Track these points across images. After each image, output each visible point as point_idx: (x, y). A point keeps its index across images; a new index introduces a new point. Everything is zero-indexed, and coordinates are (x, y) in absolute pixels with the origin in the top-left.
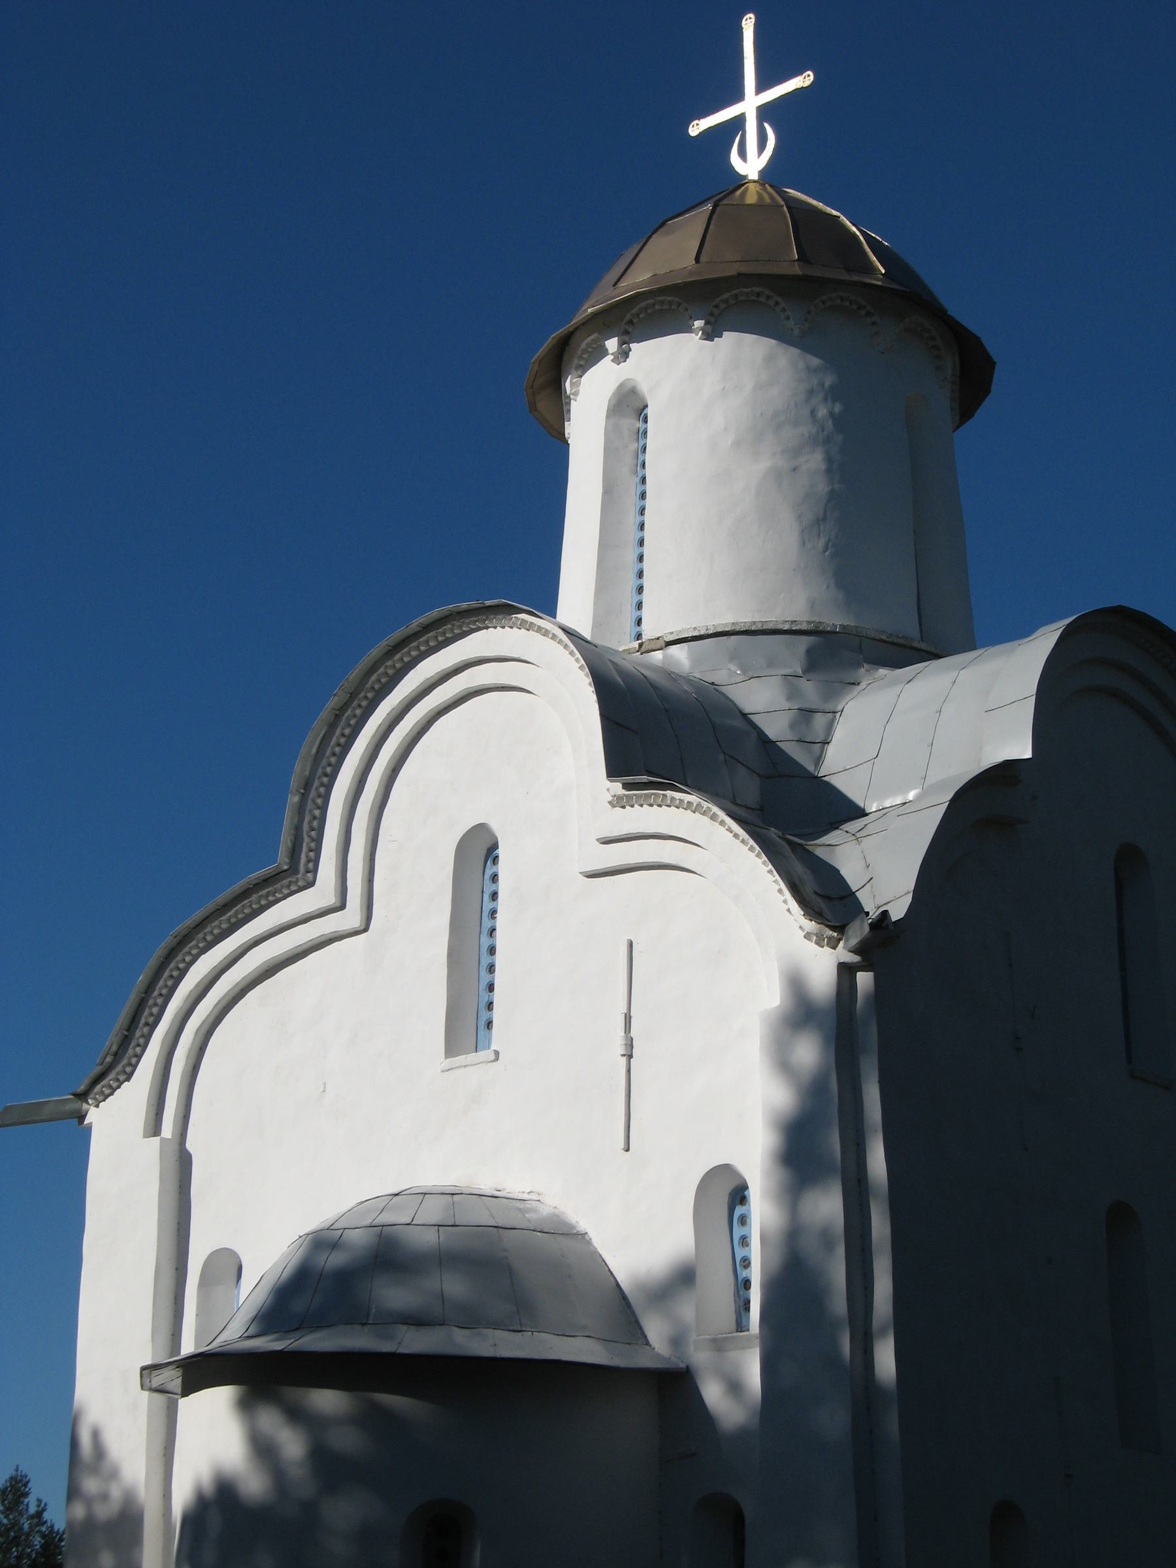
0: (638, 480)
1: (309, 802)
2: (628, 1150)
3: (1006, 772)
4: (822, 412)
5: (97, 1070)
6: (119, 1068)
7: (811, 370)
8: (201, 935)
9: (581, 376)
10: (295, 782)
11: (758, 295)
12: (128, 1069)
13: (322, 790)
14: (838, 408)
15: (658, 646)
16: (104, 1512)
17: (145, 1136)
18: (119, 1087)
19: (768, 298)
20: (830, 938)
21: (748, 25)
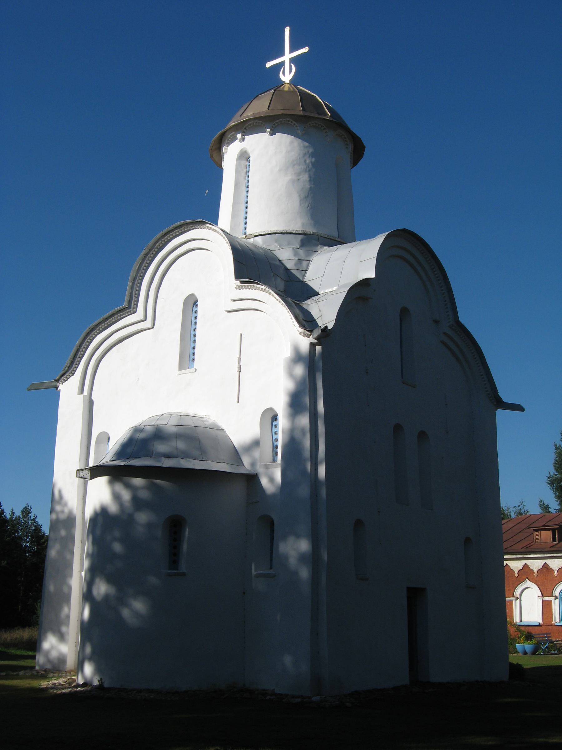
0: (246, 181)
2: (238, 402)
3: (365, 282)
4: (308, 161)
5: (63, 372)
6: (70, 372)
7: (305, 147)
8: (98, 328)
9: (228, 146)
10: (130, 278)
11: (288, 121)
12: (73, 372)
14: (313, 160)
15: (252, 237)
16: (62, 517)
18: (70, 378)
19: (292, 122)
20: (307, 334)
21: (287, 30)
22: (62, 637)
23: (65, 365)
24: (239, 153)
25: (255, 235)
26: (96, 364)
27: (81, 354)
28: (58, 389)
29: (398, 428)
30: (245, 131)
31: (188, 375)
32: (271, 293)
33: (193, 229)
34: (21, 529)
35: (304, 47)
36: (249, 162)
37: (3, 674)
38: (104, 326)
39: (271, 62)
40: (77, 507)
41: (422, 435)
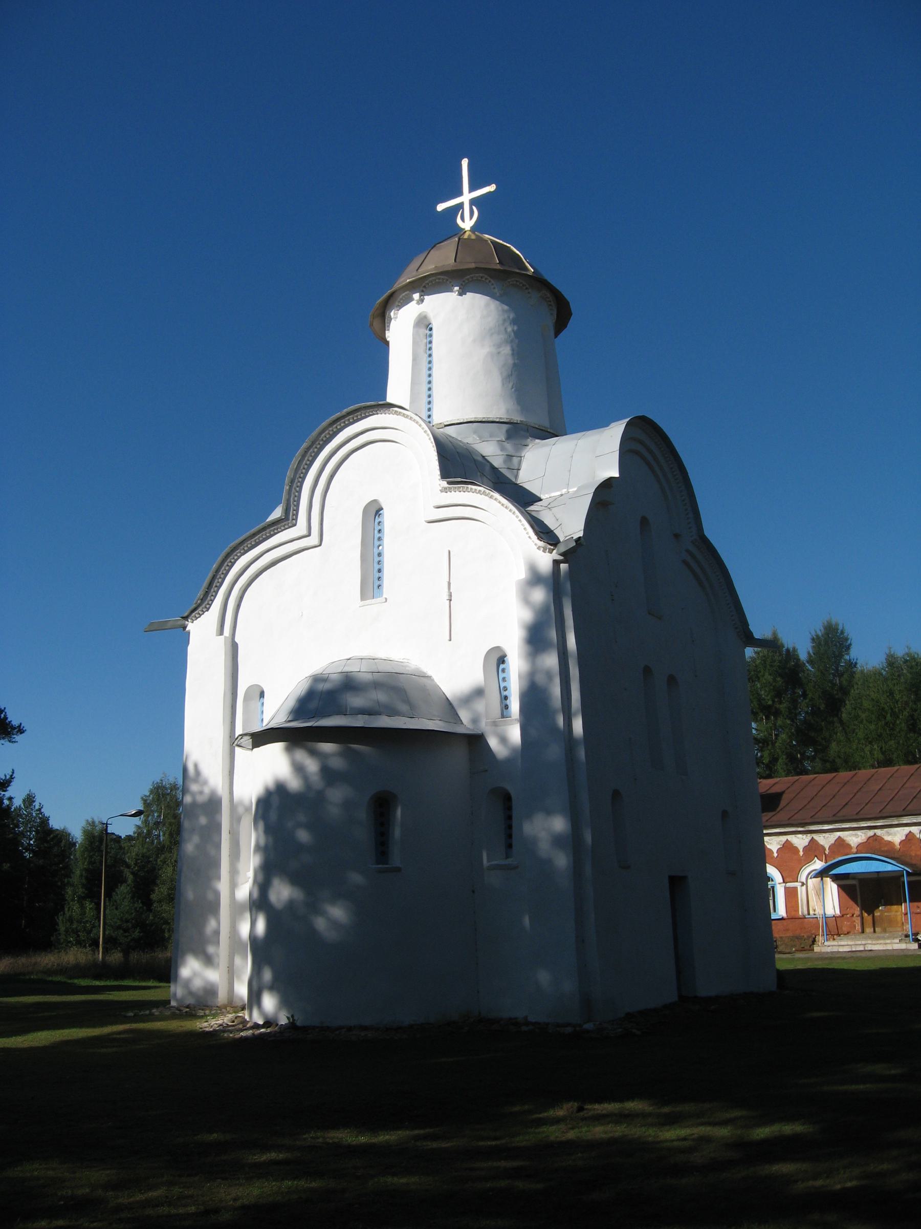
0: (427, 355)
1: (293, 490)
2: (450, 640)
3: (608, 484)
4: (509, 329)
5: (194, 606)
6: (204, 606)
7: (503, 311)
8: (242, 547)
9: (398, 310)
10: (287, 480)
12: (208, 606)
13: (299, 484)
14: (515, 328)
15: (441, 427)
16: (200, 799)
17: (217, 635)
18: (203, 614)
19: (486, 279)
20: (549, 549)
21: (465, 163)
22: (209, 961)
23: (197, 599)
24: (416, 318)
25: (445, 424)
26: (240, 595)
27: (218, 582)
28: (187, 629)
29: (647, 671)
30: (424, 289)
31: (374, 606)
32: (494, 496)
33: (374, 414)
34: (23, 822)
35: (489, 185)
36: (431, 329)
37: (131, 1014)
38: (251, 544)
39: (443, 204)
40: (222, 786)
41: (672, 680)
